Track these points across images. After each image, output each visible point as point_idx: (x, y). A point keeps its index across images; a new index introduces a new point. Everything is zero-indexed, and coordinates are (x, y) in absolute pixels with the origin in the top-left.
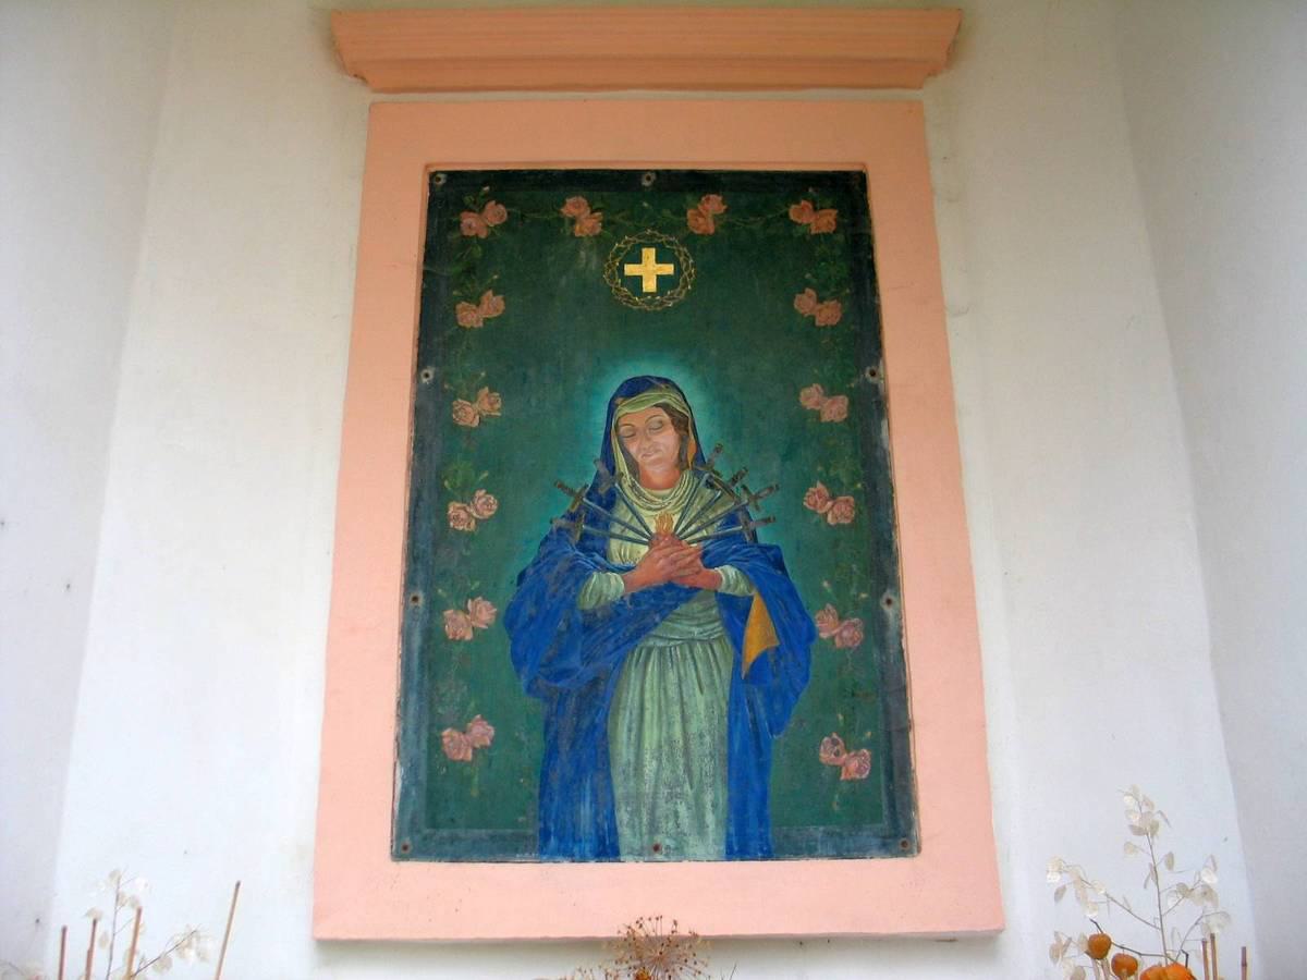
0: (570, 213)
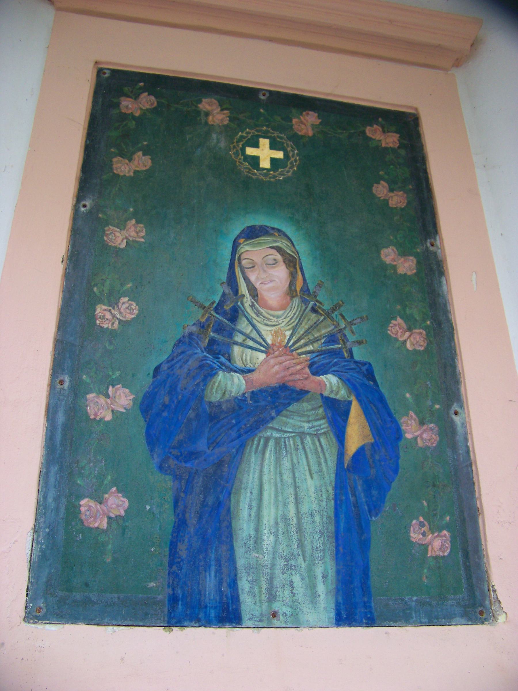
0: (205, 108)
